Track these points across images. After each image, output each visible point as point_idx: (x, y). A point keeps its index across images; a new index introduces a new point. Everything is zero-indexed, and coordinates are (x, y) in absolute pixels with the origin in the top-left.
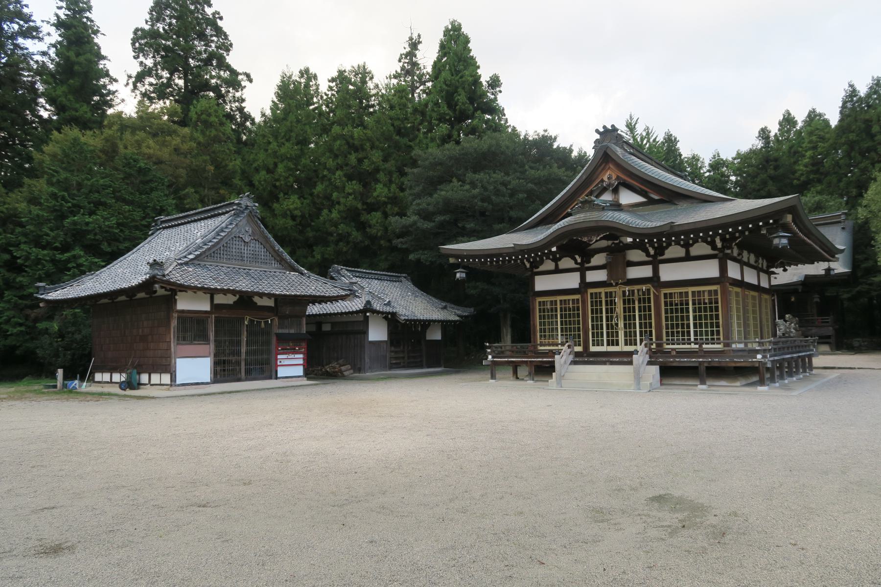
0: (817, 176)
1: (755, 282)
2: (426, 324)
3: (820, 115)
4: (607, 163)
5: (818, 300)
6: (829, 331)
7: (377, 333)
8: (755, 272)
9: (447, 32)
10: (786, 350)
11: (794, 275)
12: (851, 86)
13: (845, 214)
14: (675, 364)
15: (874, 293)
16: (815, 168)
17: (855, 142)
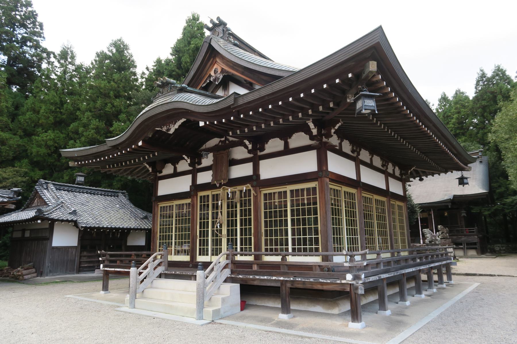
0: (462, 131)
1: (382, 186)
2: (125, 232)
3: (463, 93)
4: (214, 58)
5: (465, 215)
6: (475, 239)
7: (63, 239)
8: (383, 176)
9: (189, 21)
10: (403, 264)
11: (446, 195)
12: (482, 71)
13: (481, 151)
14: (256, 283)
15: (507, 211)
16: (460, 126)
17: (486, 106)
